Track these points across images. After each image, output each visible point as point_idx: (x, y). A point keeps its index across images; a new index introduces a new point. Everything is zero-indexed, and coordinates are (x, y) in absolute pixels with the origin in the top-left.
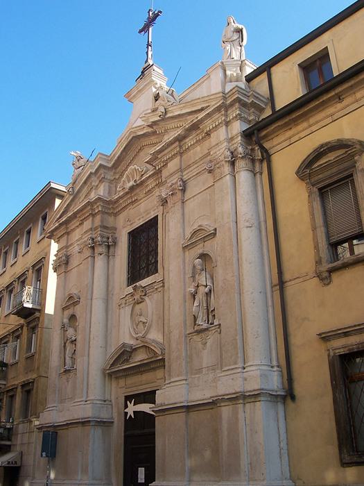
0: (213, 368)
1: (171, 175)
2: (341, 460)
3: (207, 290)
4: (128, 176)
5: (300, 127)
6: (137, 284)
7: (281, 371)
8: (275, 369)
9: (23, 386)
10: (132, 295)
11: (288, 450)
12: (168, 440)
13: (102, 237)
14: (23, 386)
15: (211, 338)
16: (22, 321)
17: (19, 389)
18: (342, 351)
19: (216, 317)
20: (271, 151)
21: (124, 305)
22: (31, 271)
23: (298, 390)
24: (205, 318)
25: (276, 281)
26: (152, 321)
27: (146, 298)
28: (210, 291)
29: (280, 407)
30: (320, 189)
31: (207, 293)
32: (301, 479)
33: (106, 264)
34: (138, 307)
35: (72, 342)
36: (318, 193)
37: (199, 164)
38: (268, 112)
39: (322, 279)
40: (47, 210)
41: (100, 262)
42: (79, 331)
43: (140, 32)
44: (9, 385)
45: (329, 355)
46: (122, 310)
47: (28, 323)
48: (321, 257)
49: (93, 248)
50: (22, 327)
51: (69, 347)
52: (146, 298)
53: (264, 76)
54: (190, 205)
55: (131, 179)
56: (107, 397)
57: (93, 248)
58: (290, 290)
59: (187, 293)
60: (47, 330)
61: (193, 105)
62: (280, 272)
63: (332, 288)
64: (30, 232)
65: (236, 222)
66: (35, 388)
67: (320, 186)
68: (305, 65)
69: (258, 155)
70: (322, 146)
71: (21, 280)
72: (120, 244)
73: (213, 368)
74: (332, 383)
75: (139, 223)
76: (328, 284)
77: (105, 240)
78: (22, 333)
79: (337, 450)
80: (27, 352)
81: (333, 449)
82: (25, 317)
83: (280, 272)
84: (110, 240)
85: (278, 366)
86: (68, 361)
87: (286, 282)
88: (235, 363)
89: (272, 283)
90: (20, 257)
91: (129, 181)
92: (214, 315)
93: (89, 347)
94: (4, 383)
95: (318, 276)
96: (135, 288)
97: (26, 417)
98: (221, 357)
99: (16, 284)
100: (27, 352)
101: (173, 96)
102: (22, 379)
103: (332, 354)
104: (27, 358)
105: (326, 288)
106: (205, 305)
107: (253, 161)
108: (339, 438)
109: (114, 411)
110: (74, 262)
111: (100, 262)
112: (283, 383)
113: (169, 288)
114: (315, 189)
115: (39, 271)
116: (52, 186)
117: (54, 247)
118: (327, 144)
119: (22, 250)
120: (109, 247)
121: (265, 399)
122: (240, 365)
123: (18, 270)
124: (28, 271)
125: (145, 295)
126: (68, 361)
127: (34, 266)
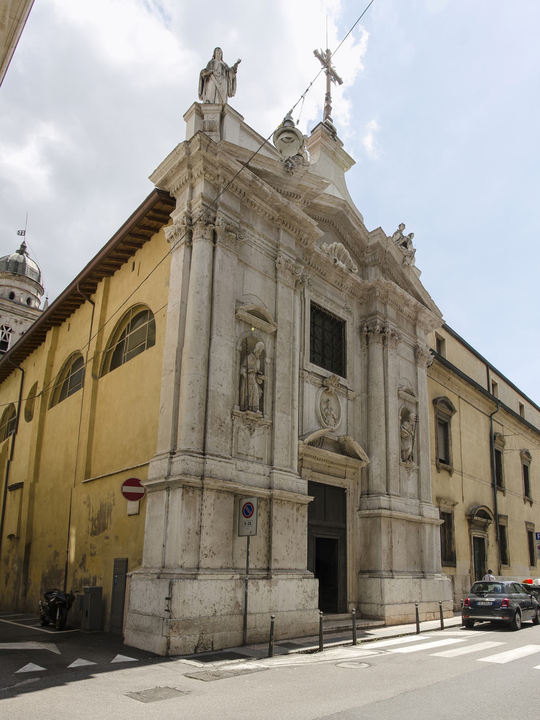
12: (394, 539)
118: (449, 399)
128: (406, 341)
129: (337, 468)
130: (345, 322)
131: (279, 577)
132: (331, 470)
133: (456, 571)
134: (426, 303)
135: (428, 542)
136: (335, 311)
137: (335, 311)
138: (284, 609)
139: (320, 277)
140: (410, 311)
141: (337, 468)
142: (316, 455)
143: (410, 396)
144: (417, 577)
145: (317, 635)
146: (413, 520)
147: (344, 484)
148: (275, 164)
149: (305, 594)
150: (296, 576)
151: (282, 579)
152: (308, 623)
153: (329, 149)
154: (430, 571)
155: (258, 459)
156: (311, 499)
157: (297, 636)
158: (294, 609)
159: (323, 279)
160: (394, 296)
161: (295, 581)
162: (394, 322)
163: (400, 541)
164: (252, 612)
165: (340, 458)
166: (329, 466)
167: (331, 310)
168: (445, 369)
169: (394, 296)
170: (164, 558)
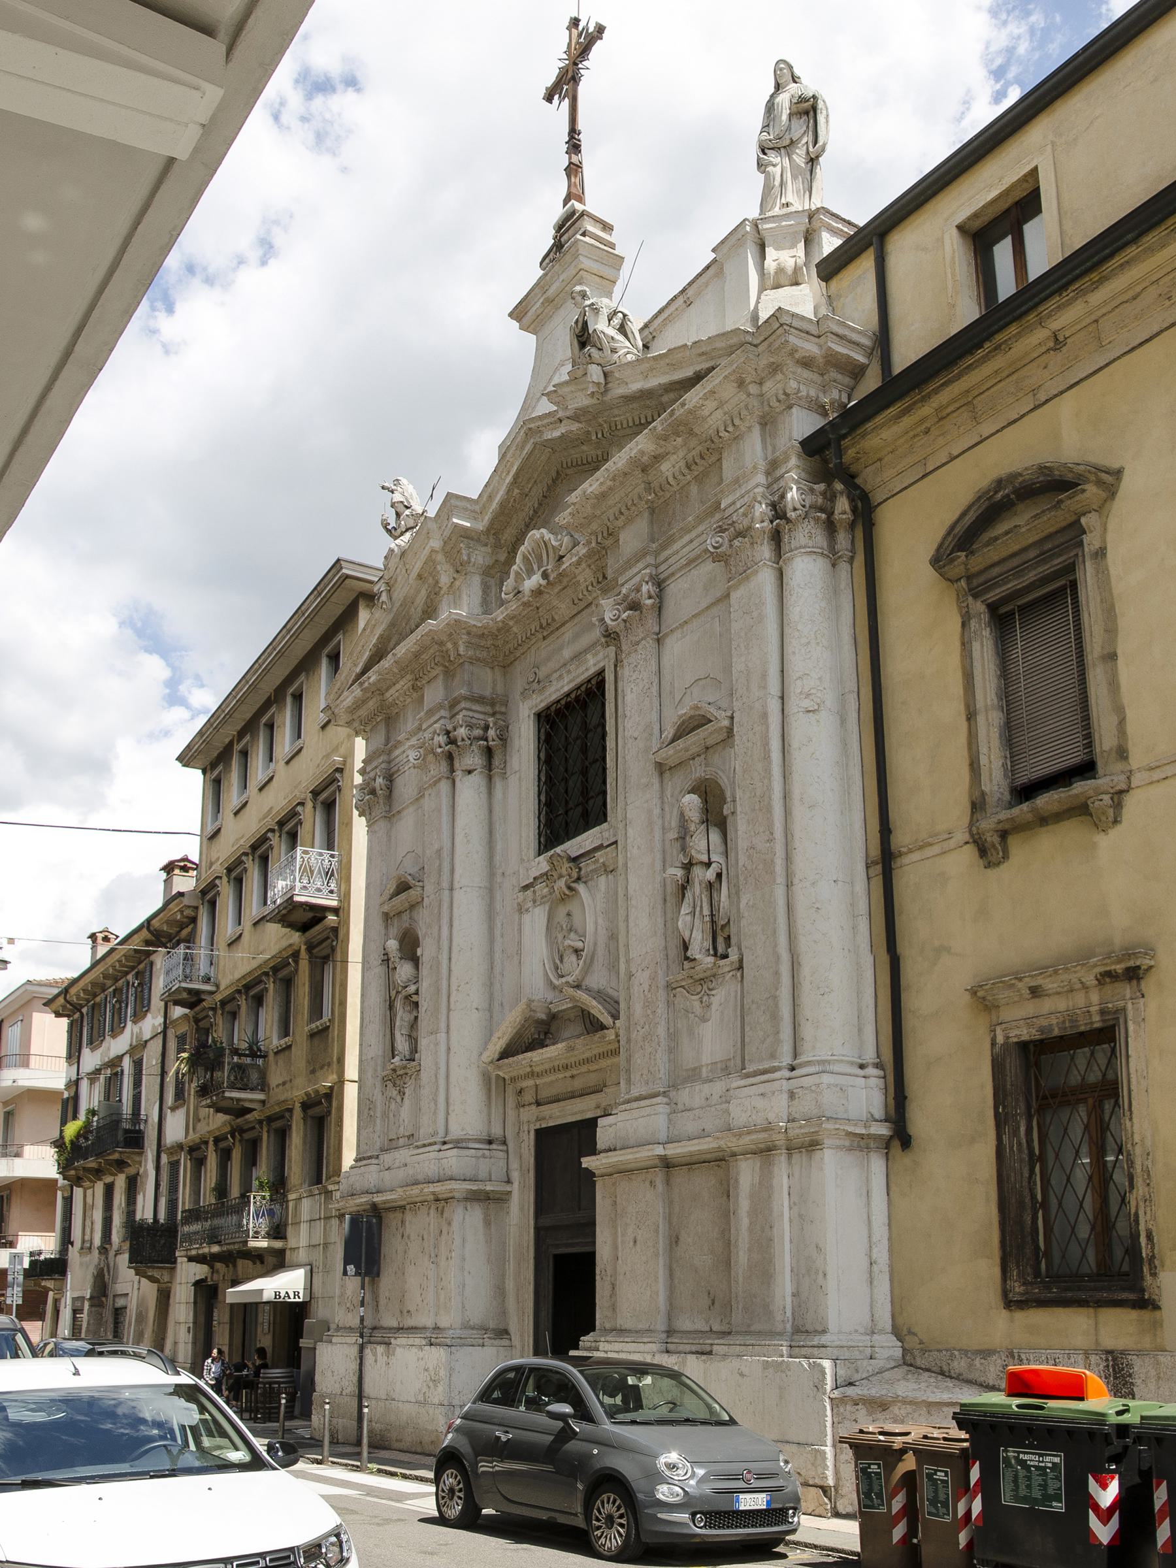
0: (725, 1069)
1: (629, 564)
2: (1005, 1293)
3: (710, 874)
4: (525, 558)
5: (1151, 236)
6: (558, 850)
7: (884, 1077)
8: (871, 1071)
9: (305, 1106)
10: (546, 876)
11: (891, 1266)
12: (623, 1235)
13: (470, 726)
14: (305, 1106)
15: (722, 995)
16: (296, 938)
17: (298, 1113)
18: (1025, 1033)
19: (733, 941)
20: (877, 497)
21: (530, 904)
22: (309, 805)
23: (920, 1123)
24: (708, 944)
25: (875, 852)
26: (595, 944)
27: (581, 888)
28: (719, 875)
29: (877, 1164)
30: (992, 608)
31: (710, 884)
32: (915, 1334)
33: (484, 796)
34: (562, 911)
35: (408, 997)
36: (985, 617)
37: (693, 534)
38: (872, 382)
39: (983, 851)
40: (341, 637)
41: (470, 790)
42: (425, 970)
43: (549, 98)
44: (272, 1101)
45: (993, 1043)
46: (526, 918)
47: (310, 948)
48: (983, 794)
49: (450, 757)
50: (296, 955)
51: (403, 1016)
52: (581, 888)
53: (866, 265)
54: (675, 647)
55: (535, 567)
56: (497, 1131)
57: (450, 757)
58: (909, 874)
59: (668, 882)
60: (693, 397)
61: (673, 366)
62: (886, 830)
63: (1005, 871)
64: (301, 695)
65: (782, 698)
66: (333, 1111)
67: (993, 595)
68: (978, 224)
69: (842, 505)
70: (999, 483)
71: (287, 827)
72: (516, 743)
73: (725, 1069)
74: (996, 1108)
75: (560, 687)
76: (998, 864)
77: (478, 732)
78: (297, 970)
79: (997, 1271)
80: (311, 1020)
81: (990, 1269)
82: (304, 928)
83: (886, 830)
84: (491, 733)
85: (878, 1066)
86: (402, 1045)
87: (901, 854)
88: (773, 1056)
89: (867, 856)
90: (279, 766)
91: (530, 572)
92: (729, 936)
93: (449, 1010)
94: (261, 1096)
95: (975, 842)
96: (551, 861)
97: (318, 1180)
98: (743, 1041)
99: (275, 840)
100: (311, 1020)
101: (626, 335)
102: (298, 1091)
103: (1000, 1039)
104: (312, 1035)
105: (992, 873)
106: (706, 912)
107: (830, 527)
108: (1003, 1242)
109: (514, 1165)
110: (407, 785)
111: (470, 790)
112: (886, 1106)
113: (626, 865)
114: (979, 607)
115: (329, 807)
116: (344, 571)
117: (360, 747)
118: (1013, 476)
119: (284, 743)
120: (489, 752)
121: (838, 1142)
122: (787, 1060)
123: (276, 801)
124: (302, 804)
125: (579, 879)
126: (402, 1045)
127: (315, 793)
128: (692, 555)
129: (589, 1071)
130: (539, 715)
131: (399, 1341)
132: (578, 1084)
133: (1157, 1325)
134: (689, 372)
135: (745, 1222)
136: (578, 676)
137: (578, 676)
138: (402, 1399)
139: (552, 632)
140: (681, 454)
141: (589, 1071)
142: (594, 1052)
143: (701, 733)
144: (694, 1348)
145: (434, 1456)
146: (704, 1157)
147: (603, 1105)
148: (373, 622)
149: (426, 1373)
150: (418, 1341)
151: (403, 1346)
152: (426, 1430)
153: (539, 312)
154: (756, 1327)
155: (409, 1137)
156: (587, 1162)
157: (413, 1450)
158: (413, 1400)
159: (557, 629)
160: (611, 502)
161: (414, 1350)
162: (638, 561)
163: (639, 1238)
164: (372, 1395)
165: (556, 1054)
166: (572, 1077)
167: (572, 685)
168: (970, 368)
169: (611, 502)
170: (1096, 1324)
